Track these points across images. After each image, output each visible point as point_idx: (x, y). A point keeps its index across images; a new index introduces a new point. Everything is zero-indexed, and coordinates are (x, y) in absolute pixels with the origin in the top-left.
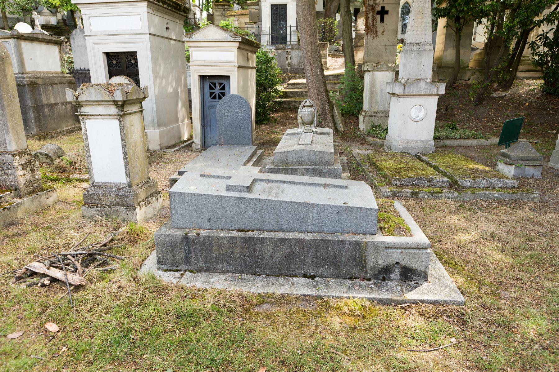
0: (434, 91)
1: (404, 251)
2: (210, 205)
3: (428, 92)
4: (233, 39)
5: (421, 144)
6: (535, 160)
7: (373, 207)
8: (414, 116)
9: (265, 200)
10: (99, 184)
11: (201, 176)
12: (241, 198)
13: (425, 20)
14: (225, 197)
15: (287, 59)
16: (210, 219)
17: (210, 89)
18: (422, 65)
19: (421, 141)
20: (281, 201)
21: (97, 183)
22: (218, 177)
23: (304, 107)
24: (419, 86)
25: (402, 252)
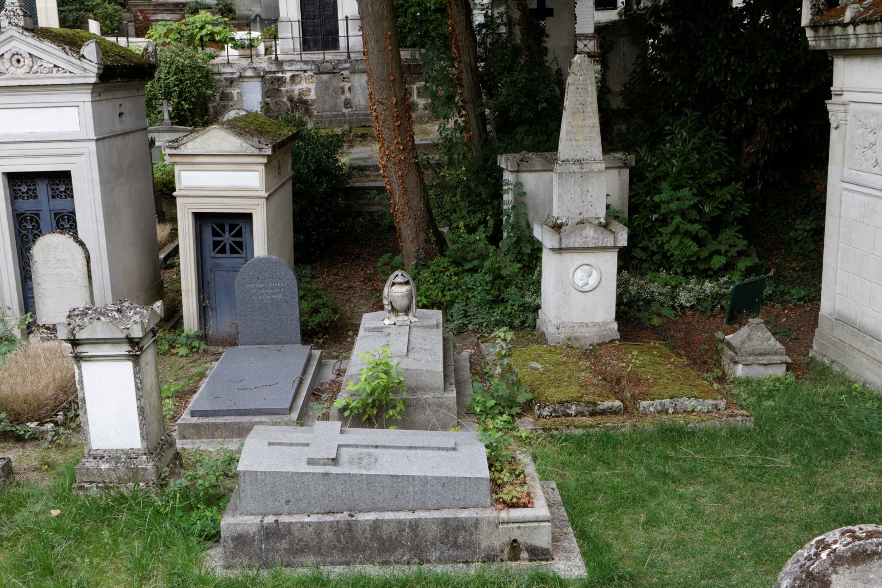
0: (609, 242)
1: (521, 525)
2: (289, 484)
3: (600, 244)
4: (257, 152)
5: (594, 329)
6: (772, 355)
7: (483, 476)
8: (580, 283)
9: (355, 475)
10: (99, 452)
11: (270, 444)
12: (327, 474)
13: (589, 122)
14: (307, 473)
15: (343, 92)
16: (289, 501)
17: (225, 253)
18: (589, 196)
19: (595, 325)
20: (375, 475)
21: (96, 450)
22: (292, 444)
23: (394, 284)
24: (584, 235)
25: (519, 527)
